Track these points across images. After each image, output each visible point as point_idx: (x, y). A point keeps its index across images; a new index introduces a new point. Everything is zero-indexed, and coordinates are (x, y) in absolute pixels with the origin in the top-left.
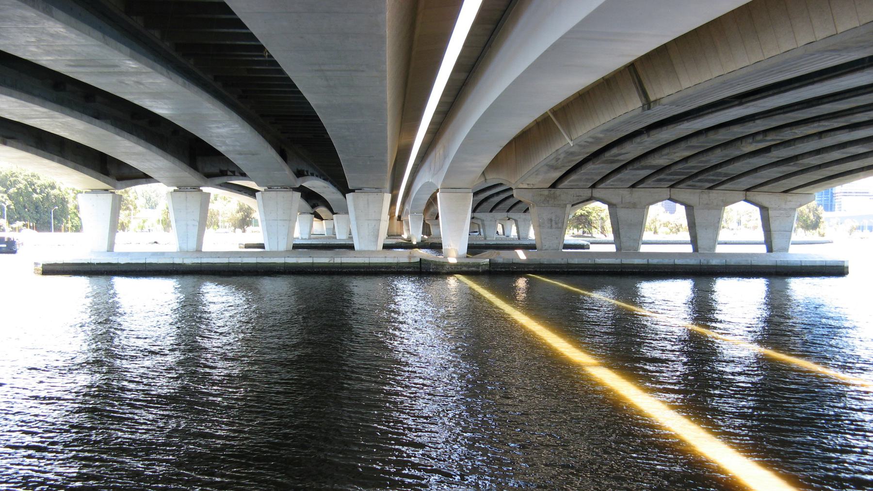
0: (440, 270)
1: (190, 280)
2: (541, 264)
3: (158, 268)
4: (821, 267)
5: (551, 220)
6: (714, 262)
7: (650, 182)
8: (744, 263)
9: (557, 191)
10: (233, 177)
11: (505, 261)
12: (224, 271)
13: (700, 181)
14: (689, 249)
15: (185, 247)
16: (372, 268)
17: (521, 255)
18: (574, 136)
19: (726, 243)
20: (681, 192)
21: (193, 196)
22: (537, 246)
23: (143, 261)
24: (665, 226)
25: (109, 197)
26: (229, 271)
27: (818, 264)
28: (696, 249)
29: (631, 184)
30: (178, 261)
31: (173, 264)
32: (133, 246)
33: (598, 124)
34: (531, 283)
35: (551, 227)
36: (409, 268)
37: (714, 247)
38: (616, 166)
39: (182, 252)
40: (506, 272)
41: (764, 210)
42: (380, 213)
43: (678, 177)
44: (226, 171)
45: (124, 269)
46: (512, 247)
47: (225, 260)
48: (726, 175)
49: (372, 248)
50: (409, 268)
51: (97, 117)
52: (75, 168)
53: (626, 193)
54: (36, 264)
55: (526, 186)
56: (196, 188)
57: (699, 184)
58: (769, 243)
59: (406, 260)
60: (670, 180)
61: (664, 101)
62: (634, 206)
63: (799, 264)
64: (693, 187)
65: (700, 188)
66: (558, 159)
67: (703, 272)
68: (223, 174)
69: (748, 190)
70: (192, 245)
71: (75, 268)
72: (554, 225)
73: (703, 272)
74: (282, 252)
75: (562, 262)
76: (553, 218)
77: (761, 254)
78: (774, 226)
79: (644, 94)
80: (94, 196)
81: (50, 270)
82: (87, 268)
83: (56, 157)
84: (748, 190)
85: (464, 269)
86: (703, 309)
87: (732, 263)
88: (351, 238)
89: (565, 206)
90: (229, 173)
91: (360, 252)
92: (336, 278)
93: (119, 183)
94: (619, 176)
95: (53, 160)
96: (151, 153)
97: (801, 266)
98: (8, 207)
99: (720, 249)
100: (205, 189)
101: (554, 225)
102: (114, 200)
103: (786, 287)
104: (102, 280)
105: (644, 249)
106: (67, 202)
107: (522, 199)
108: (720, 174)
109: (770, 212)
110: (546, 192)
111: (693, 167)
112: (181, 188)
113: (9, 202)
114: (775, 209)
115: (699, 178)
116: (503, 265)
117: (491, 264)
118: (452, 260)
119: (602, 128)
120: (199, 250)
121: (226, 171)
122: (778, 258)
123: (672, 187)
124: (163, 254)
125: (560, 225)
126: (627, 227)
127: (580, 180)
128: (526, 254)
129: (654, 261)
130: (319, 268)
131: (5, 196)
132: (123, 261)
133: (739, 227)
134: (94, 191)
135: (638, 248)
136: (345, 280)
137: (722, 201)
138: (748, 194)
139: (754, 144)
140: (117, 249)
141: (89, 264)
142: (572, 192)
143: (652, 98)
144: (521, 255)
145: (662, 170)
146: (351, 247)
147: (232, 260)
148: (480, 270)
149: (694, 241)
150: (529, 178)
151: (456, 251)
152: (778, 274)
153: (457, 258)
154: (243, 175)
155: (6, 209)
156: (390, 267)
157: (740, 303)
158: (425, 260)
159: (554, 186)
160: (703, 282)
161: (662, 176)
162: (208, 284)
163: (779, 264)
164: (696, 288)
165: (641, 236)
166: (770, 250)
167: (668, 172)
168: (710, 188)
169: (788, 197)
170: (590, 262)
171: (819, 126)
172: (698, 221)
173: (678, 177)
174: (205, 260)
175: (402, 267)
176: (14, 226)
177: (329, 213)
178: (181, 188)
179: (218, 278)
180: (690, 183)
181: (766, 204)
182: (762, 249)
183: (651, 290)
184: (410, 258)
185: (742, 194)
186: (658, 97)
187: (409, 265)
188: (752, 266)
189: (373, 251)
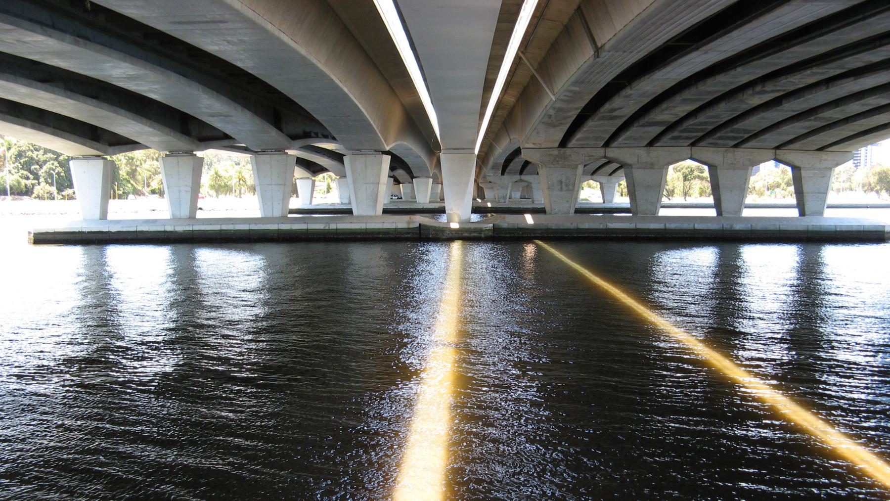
0: (440, 235)
1: (183, 248)
2: (548, 229)
3: (149, 236)
4: (858, 232)
5: (561, 182)
6: (738, 227)
7: (666, 139)
8: (771, 228)
9: (568, 151)
10: (317, 139)
11: (510, 227)
12: (216, 239)
13: (720, 138)
14: (712, 213)
15: (177, 213)
16: (369, 234)
17: (529, 219)
18: (556, 91)
19: (867, 207)
20: (702, 151)
21: (186, 161)
22: (547, 209)
23: (133, 229)
24: (685, 190)
25: (100, 163)
26: (222, 239)
27: (855, 229)
28: (719, 213)
29: (646, 143)
30: (169, 228)
31: (165, 232)
32: (128, 212)
33: (569, 76)
34: (539, 249)
35: (561, 189)
36: (408, 233)
37: (740, 211)
38: (620, 122)
39: (175, 219)
40: (511, 237)
41: (796, 169)
42: (379, 175)
43: (695, 134)
44: (310, 133)
45: (115, 237)
46: (522, 211)
47: (217, 227)
48: (745, 131)
49: (370, 213)
50: (408, 233)
51: (184, 76)
52: (53, 134)
53: (642, 152)
54: (29, 233)
55: (532, 146)
56: (190, 153)
57: (721, 142)
58: (801, 206)
59: (404, 226)
60: (735, 138)
61: (607, 47)
62: (652, 166)
63: (833, 229)
64: (715, 145)
65: (724, 146)
66: (550, 116)
67: (729, 238)
68: (306, 135)
69: (778, 148)
70: (185, 212)
71: (66, 237)
72: (564, 188)
73: (729, 238)
74: (276, 218)
75: (572, 227)
76: (563, 180)
77: (792, 219)
78: (806, 187)
79: (593, 41)
80: (84, 162)
81: (41, 239)
82: (78, 237)
83: (29, 123)
84: (778, 148)
85: (466, 235)
86: (727, 278)
87: (758, 228)
88: (350, 203)
89: (576, 167)
90: (313, 135)
91: (358, 217)
92: (333, 247)
93: (111, 149)
94: (628, 134)
95: (24, 125)
96: (120, 117)
97: (836, 231)
98: (58, 174)
99: (746, 213)
100: (199, 154)
101: (564, 188)
102: (105, 166)
103: (738, 256)
104: (93, 249)
105: (663, 212)
106: (118, 169)
107: (529, 160)
108: (738, 131)
109: (802, 172)
110: (556, 152)
111: (705, 123)
112: (173, 153)
113: (59, 169)
114: (809, 169)
115: (718, 135)
116: (508, 230)
117: (496, 229)
118: (455, 226)
119: (572, 80)
120: (192, 217)
121: (310, 133)
122: (811, 223)
123: (693, 145)
124: (155, 221)
125: (571, 187)
126: (647, 190)
127: (587, 138)
128: (525, 219)
129: (672, 226)
130: (313, 234)
131: (56, 163)
132: (114, 229)
133: (768, 188)
134: (85, 157)
135: (656, 211)
136: (342, 247)
137: (749, 160)
138: (778, 152)
139: (757, 97)
140: (110, 217)
141: (79, 232)
142: (583, 152)
143: (599, 45)
144: (529, 219)
145: (671, 127)
146: (349, 212)
147: (224, 227)
148: (483, 236)
149: (718, 205)
150: (535, 137)
151: (458, 215)
152: (812, 239)
153: (460, 223)
154: (328, 137)
155: (55, 176)
156: (388, 233)
157: (769, 273)
158: (425, 226)
159: (563, 143)
160: (811, 247)
161: (676, 134)
162: (823, 248)
163: (810, 228)
164: (804, 254)
165: (659, 199)
166: (802, 213)
167: (680, 128)
168: (736, 146)
169: (823, 155)
170: (601, 227)
171: (815, 74)
172: (722, 181)
173: (695, 134)
174: (196, 228)
175: (401, 233)
176: (64, 193)
177: (407, 177)
178: (173, 153)
179: (240, 245)
180: (710, 140)
181: (797, 164)
182: (794, 213)
183: (752, 255)
184: (409, 223)
185: (771, 153)
186: (603, 42)
187: (408, 231)
188: (780, 231)
189: (371, 217)
